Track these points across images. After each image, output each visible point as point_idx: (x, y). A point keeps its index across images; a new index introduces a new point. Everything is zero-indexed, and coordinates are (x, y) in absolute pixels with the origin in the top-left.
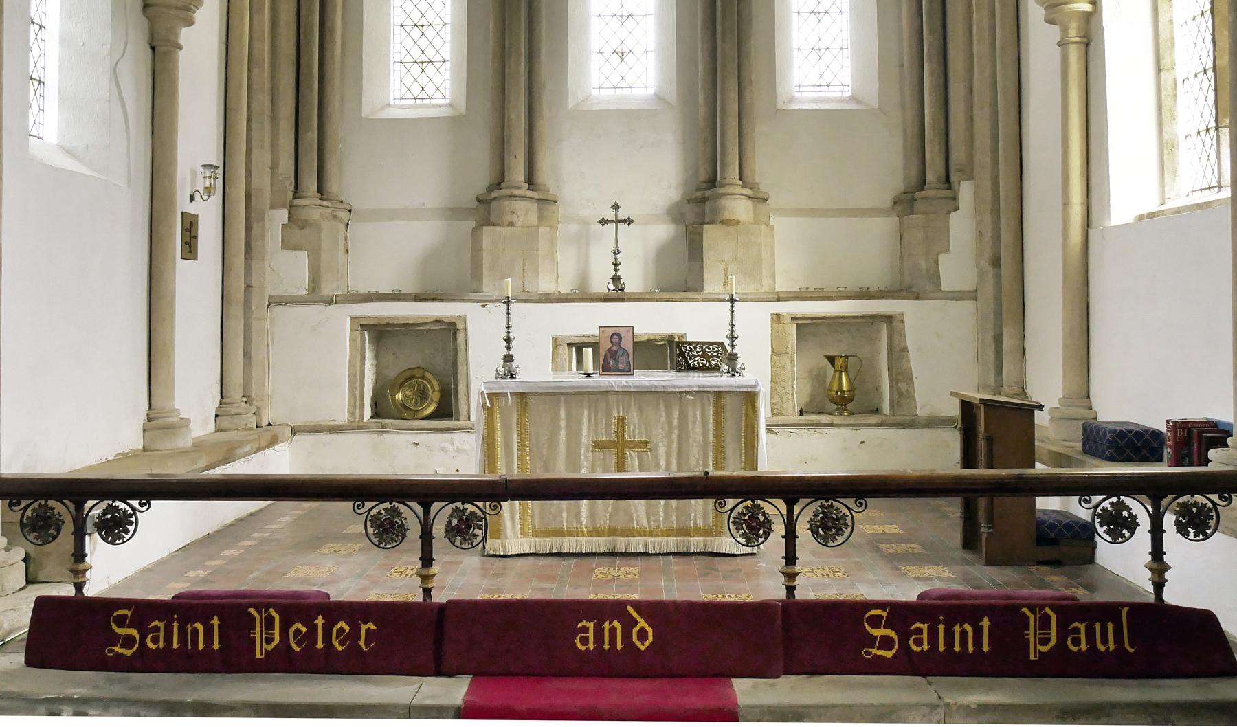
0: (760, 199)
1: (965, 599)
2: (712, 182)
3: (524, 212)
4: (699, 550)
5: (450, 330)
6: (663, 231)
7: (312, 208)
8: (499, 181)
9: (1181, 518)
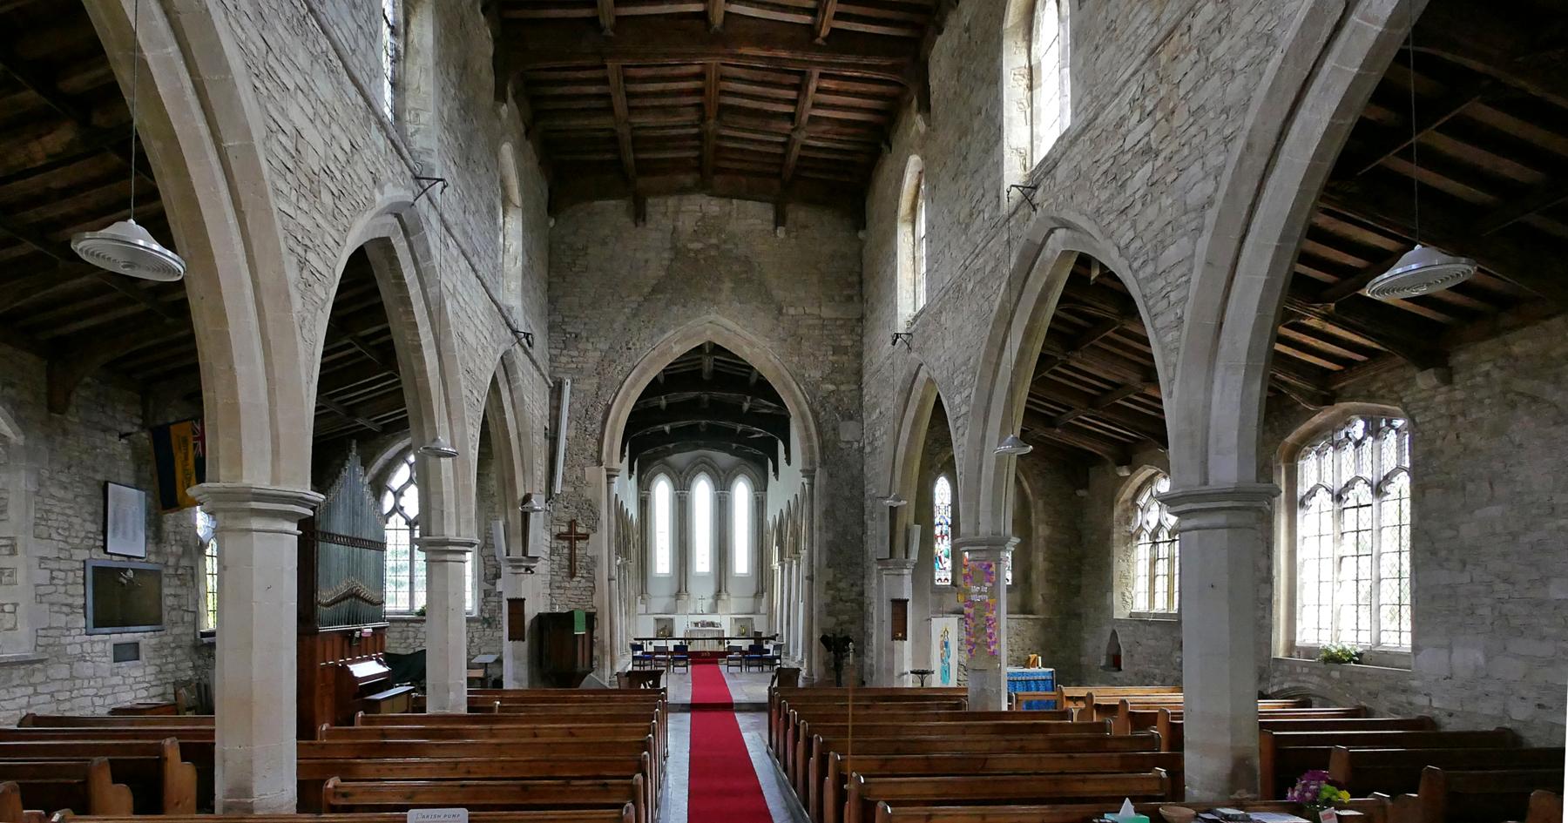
0: (728, 595)
1: (811, 447)
2: (720, 591)
3: (685, 597)
4: (1020, 286)
5: (672, 620)
6: (711, 600)
7: (645, 595)
8: (679, 591)
9: (819, 41)
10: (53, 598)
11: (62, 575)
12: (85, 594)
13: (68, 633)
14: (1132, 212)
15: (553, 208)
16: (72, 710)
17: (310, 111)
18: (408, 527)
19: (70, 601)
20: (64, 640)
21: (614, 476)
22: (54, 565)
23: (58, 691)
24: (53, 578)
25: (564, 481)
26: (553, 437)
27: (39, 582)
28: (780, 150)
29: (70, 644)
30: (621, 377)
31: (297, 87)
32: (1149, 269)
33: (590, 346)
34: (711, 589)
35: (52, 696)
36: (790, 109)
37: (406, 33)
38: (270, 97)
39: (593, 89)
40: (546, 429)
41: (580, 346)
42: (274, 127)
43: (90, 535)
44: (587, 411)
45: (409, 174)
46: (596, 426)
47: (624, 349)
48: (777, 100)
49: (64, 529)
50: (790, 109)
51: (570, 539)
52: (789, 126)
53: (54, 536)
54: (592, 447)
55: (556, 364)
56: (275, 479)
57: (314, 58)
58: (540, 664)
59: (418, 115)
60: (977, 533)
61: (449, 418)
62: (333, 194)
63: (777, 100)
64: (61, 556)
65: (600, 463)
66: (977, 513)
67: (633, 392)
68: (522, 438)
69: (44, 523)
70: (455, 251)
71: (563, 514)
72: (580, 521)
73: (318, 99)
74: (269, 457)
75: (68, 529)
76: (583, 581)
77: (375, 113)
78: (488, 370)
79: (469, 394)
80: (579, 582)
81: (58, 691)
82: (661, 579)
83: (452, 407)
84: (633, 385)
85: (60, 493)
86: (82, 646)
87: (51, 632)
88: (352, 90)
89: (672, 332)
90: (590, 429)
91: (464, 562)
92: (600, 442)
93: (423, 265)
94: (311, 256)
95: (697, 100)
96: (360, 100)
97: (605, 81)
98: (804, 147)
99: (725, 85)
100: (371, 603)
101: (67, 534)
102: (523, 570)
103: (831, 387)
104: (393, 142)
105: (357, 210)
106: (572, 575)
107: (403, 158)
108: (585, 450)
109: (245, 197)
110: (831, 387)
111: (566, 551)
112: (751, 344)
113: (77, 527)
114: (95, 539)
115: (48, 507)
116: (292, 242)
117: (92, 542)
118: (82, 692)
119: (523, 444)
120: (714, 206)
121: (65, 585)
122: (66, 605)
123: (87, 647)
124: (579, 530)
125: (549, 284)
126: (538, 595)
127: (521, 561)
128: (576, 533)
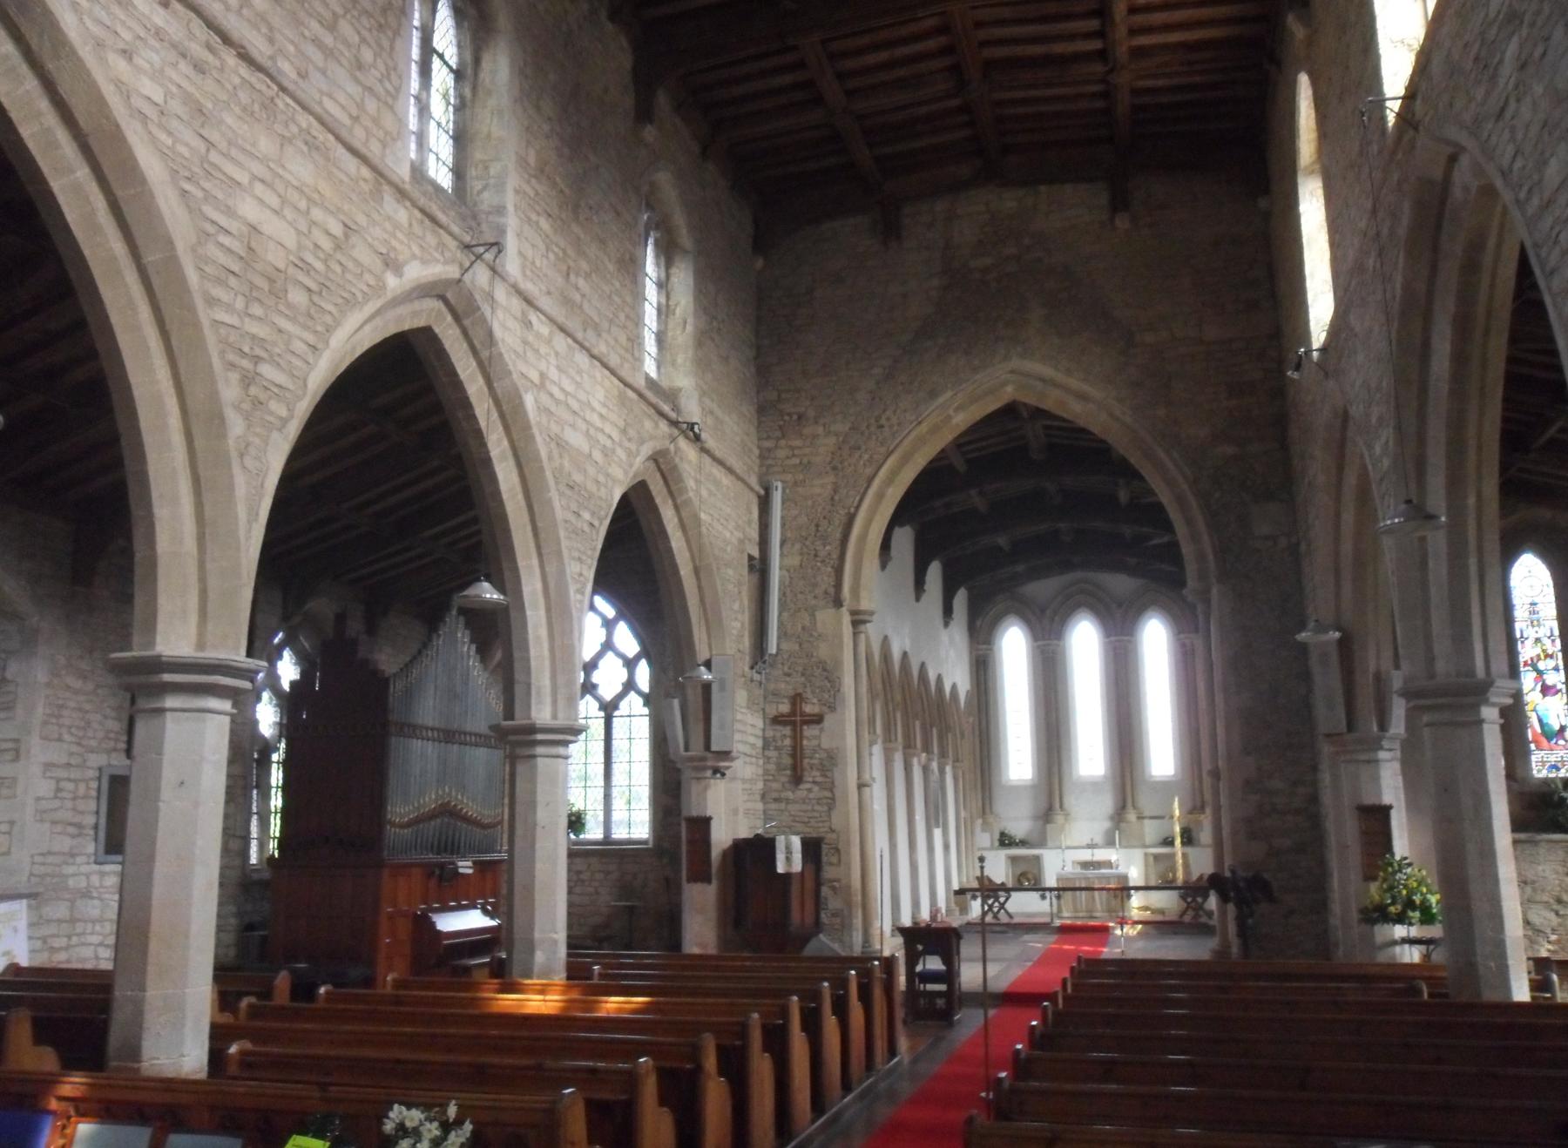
5: (1038, 859)
10: (60, 815)
11: (70, 786)
12: (97, 813)
13: (71, 861)
14: (1508, 114)
15: (761, 243)
16: (68, 961)
17: (274, 201)
18: (602, 714)
19: (77, 819)
20: (70, 870)
21: (864, 622)
22: (62, 773)
23: (53, 936)
24: (58, 790)
25: (783, 634)
26: (759, 568)
27: (41, 794)
28: (1100, 104)
29: (74, 875)
30: (869, 471)
31: (254, 178)
32: (1535, 201)
33: (820, 430)
34: (1106, 803)
35: (45, 942)
36: (1096, 45)
37: (476, 74)
38: (208, 197)
39: (788, 79)
40: (751, 558)
41: (807, 431)
42: (210, 229)
43: (112, 735)
44: (817, 526)
45: (452, 244)
46: (832, 548)
47: (873, 429)
48: (1072, 37)
49: (78, 728)
50: (1096, 45)
51: (793, 724)
52: (1098, 68)
53: (66, 737)
54: (826, 581)
55: (770, 462)
56: (201, 645)
57: (285, 141)
58: (738, 922)
59: (486, 168)
60: (1432, 676)
61: (540, 555)
62: (309, 290)
63: (1072, 37)
64: (73, 762)
65: (838, 603)
66: (1428, 637)
67: (890, 491)
68: (702, 575)
69: (54, 721)
70: (544, 329)
71: (783, 686)
72: (809, 695)
73: (288, 184)
74: (193, 619)
75: (84, 729)
76: (816, 788)
77: (391, 183)
78: (614, 481)
79: (573, 518)
80: (810, 790)
81: (53, 936)
82: (1016, 789)
83: (542, 536)
84: (889, 481)
85: (78, 684)
86: (88, 878)
87: (50, 859)
88: (351, 164)
89: (949, 394)
90: (822, 554)
91: (566, 758)
92: (839, 572)
93: (485, 354)
94: (266, 370)
95: (947, 61)
96: (365, 172)
97: (801, 65)
98: (1135, 92)
99: (982, 34)
100: (484, 827)
101: (81, 734)
102: (709, 773)
103: (1230, 450)
104: (423, 211)
105: (350, 303)
106: (797, 779)
107: (441, 226)
108: (815, 585)
109: (169, 312)
110: (1230, 450)
111: (788, 742)
112: (1082, 397)
113: (95, 725)
114: (116, 740)
115: (60, 702)
116: (231, 357)
117: (112, 744)
118: (83, 940)
119: (704, 583)
120: (1008, 201)
121: (74, 799)
122: (71, 824)
123: (95, 880)
124: (808, 709)
125: (759, 348)
126: (735, 812)
127: (703, 759)
128: (803, 714)
